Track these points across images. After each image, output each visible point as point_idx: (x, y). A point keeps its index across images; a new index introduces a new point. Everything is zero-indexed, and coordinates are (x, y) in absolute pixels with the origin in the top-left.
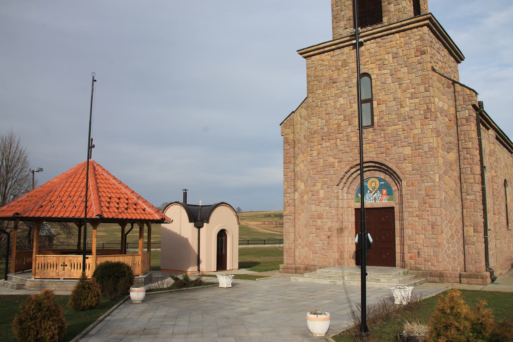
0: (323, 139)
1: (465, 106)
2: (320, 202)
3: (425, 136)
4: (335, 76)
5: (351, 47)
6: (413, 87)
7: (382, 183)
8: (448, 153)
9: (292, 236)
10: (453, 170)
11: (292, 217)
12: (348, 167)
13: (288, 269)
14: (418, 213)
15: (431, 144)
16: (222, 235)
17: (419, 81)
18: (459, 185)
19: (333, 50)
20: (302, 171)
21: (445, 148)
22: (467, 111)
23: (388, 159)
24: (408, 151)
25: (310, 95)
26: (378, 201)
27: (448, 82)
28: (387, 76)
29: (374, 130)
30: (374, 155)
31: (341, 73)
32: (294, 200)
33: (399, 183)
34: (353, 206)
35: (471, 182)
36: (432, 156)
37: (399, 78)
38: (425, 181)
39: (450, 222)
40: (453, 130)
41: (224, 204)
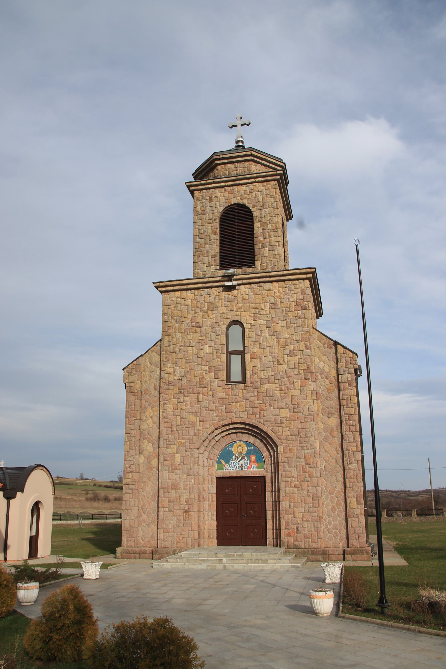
0: (181, 392)
2: (175, 469)
3: (305, 398)
4: (200, 319)
5: (221, 289)
6: (293, 343)
7: (251, 448)
8: (329, 418)
9: (135, 511)
12: (213, 428)
13: (129, 553)
14: (296, 483)
15: (312, 408)
16: (36, 507)
17: (299, 337)
18: (340, 453)
19: (199, 289)
20: (150, 429)
21: (326, 412)
22: (349, 375)
24: (285, 413)
25: (166, 338)
29: (245, 386)
30: (245, 415)
31: (207, 317)
32: (139, 465)
33: (272, 448)
35: (353, 450)
36: (313, 420)
37: (277, 332)
38: (305, 448)
40: (334, 394)
41: (41, 467)
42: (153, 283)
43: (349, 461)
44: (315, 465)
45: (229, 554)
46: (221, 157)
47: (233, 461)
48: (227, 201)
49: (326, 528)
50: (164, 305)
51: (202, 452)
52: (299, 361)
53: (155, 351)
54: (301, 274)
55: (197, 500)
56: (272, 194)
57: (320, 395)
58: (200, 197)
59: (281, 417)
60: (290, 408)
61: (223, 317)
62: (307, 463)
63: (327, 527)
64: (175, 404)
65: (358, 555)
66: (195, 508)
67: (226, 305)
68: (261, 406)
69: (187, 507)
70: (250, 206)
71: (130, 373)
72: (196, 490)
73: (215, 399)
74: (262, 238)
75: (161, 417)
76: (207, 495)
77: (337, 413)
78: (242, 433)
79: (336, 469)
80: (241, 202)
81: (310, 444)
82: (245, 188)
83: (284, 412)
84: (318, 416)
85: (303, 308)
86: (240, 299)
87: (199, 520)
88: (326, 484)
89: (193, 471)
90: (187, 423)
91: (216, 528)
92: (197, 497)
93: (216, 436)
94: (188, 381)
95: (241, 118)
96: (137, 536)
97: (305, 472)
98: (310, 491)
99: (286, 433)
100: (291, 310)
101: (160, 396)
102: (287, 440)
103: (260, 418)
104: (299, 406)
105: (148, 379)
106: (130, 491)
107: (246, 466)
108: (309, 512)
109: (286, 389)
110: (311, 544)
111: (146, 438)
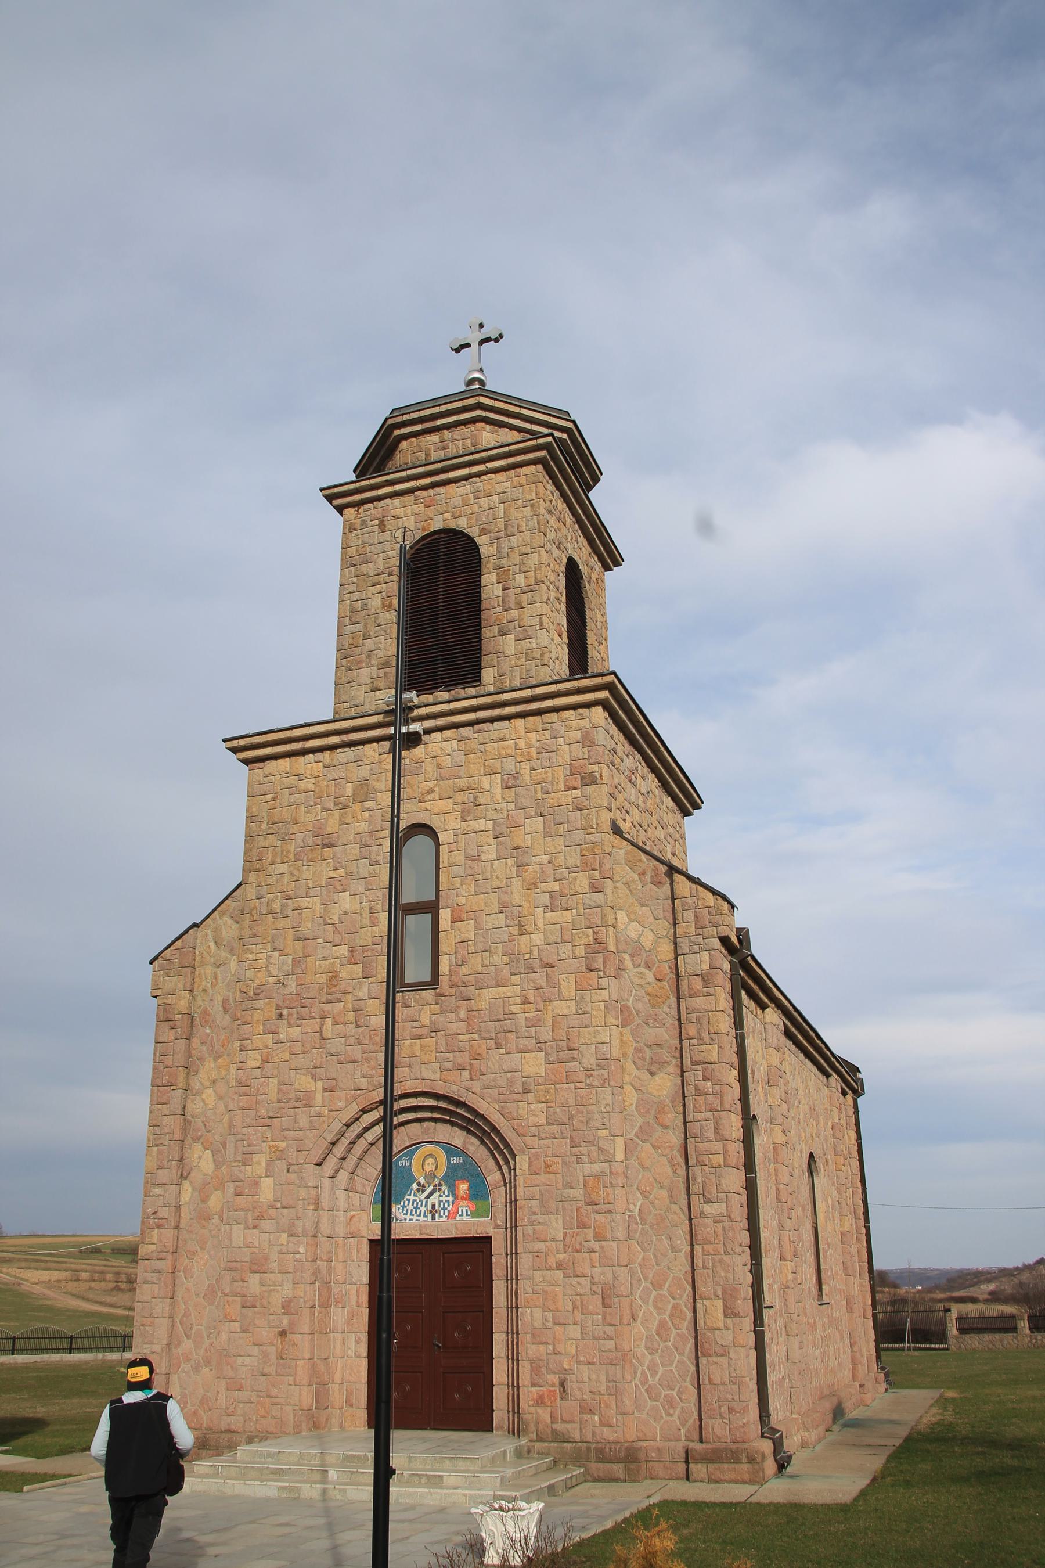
0: (281, 1015)
1: (701, 940)
2: (260, 1218)
4: (332, 825)
6: (558, 876)
7: (457, 1160)
8: (652, 1074)
10: (667, 1127)
11: (165, 1265)
12: (354, 1109)
14: (561, 1256)
15: (604, 1048)
17: (575, 859)
18: (682, 1172)
19: (332, 748)
20: (209, 1113)
21: (644, 1059)
22: (705, 955)
23: (476, 1086)
24: (535, 1064)
25: (252, 877)
29: (438, 995)
30: (434, 1072)
32: (178, 1207)
33: (507, 1162)
34: (364, 1233)
37: (518, 848)
38: (585, 1158)
39: (657, 1285)
40: (666, 1009)
42: (225, 741)
43: (704, 1195)
45: (354, 1456)
46: (406, 418)
47: (412, 1198)
48: (419, 525)
50: (251, 796)
51: (330, 1173)
56: (528, 497)
57: (631, 1013)
58: (358, 521)
59: (525, 1074)
63: (644, 1381)
65: (726, 1466)
70: (473, 532)
71: (166, 971)
73: (362, 1032)
74: (500, 609)
77: (674, 1061)
80: (452, 525)
82: (464, 488)
84: (624, 1070)
85: (587, 781)
95: (481, 326)
97: (583, 1226)
98: (596, 1280)
99: (537, 1120)
104: (572, 1046)
105: (209, 985)
106: (153, 1277)
107: (444, 1209)
108: (594, 1338)
109: (539, 999)
110: (598, 1430)
111: (199, 1138)
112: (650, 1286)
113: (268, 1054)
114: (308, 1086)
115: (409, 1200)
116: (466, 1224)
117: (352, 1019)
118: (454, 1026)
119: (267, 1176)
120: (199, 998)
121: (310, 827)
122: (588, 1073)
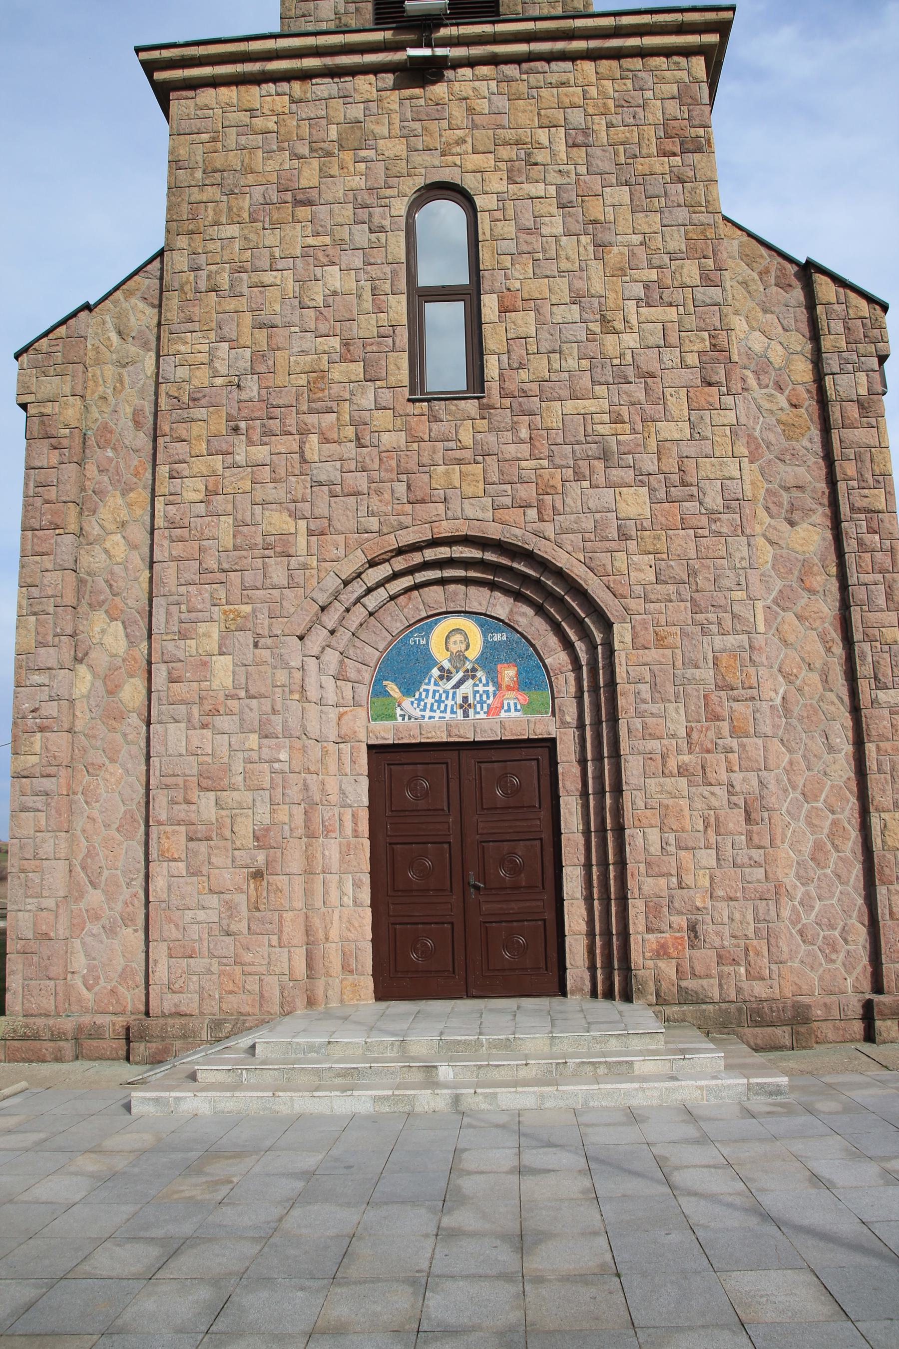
0: (236, 429)
4: (309, 175)
6: (656, 262)
7: (497, 637)
8: (792, 524)
9: (56, 877)
12: (358, 559)
13: (36, 1038)
14: (686, 758)
15: (734, 486)
17: (676, 242)
18: (839, 649)
20: (117, 569)
21: (780, 505)
22: (862, 377)
24: (635, 503)
25: (182, 242)
26: (479, 715)
27: (782, 269)
28: (543, 207)
29: (481, 407)
30: (484, 509)
31: (335, 171)
32: (72, 702)
33: (586, 635)
34: (362, 736)
36: (741, 529)
37: (595, 222)
40: (806, 443)
44: (754, 692)
47: (432, 688)
49: (794, 924)
52: (679, 321)
53: (139, 294)
54: (681, 29)
55: (301, 831)
60: (654, 484)
61: (394, 171)
62: (724, 686)
64: (214, 474)
66: (295, 862)
67: (405, 132)
68: (546, 477)
69: (261, 858)
72: (294, 793)
73: (369, 454)
75: (159, 522)
76: (336, 810)
77: (820, 510)
78: (466, 582)
79: (824, 706)
81: (734, 616)
83: (630, 500)
85: (690, 146)
86: (458, 112)
87: (309, 907)
88: (791, 763)
89: (285, 722)
90: (259, 540)
91: (370, 936)
92: (299, 819)
93: (369, 591)
94: (263, 392)
96: (66, 972)
98: (738, 789)
99: (641, 576)
100: (645, 151)
101: (155, 448)
102: (647, 600)
103: (541, 520)
104: (689, 479)
106: (39, 802)
107: (482, 702)
109: (638, 419)
110: (745, 985)
111: (101, 604)
112: (801, 798)
113: (216, 484)
114: (285, 527)
115: (427, 691)
116: (516, 721)
117: (352, 436)
118: (512, 448)
119: (221, 654)
120: (94, 409)
121: (274, 178)
122: (713, 516)
